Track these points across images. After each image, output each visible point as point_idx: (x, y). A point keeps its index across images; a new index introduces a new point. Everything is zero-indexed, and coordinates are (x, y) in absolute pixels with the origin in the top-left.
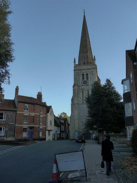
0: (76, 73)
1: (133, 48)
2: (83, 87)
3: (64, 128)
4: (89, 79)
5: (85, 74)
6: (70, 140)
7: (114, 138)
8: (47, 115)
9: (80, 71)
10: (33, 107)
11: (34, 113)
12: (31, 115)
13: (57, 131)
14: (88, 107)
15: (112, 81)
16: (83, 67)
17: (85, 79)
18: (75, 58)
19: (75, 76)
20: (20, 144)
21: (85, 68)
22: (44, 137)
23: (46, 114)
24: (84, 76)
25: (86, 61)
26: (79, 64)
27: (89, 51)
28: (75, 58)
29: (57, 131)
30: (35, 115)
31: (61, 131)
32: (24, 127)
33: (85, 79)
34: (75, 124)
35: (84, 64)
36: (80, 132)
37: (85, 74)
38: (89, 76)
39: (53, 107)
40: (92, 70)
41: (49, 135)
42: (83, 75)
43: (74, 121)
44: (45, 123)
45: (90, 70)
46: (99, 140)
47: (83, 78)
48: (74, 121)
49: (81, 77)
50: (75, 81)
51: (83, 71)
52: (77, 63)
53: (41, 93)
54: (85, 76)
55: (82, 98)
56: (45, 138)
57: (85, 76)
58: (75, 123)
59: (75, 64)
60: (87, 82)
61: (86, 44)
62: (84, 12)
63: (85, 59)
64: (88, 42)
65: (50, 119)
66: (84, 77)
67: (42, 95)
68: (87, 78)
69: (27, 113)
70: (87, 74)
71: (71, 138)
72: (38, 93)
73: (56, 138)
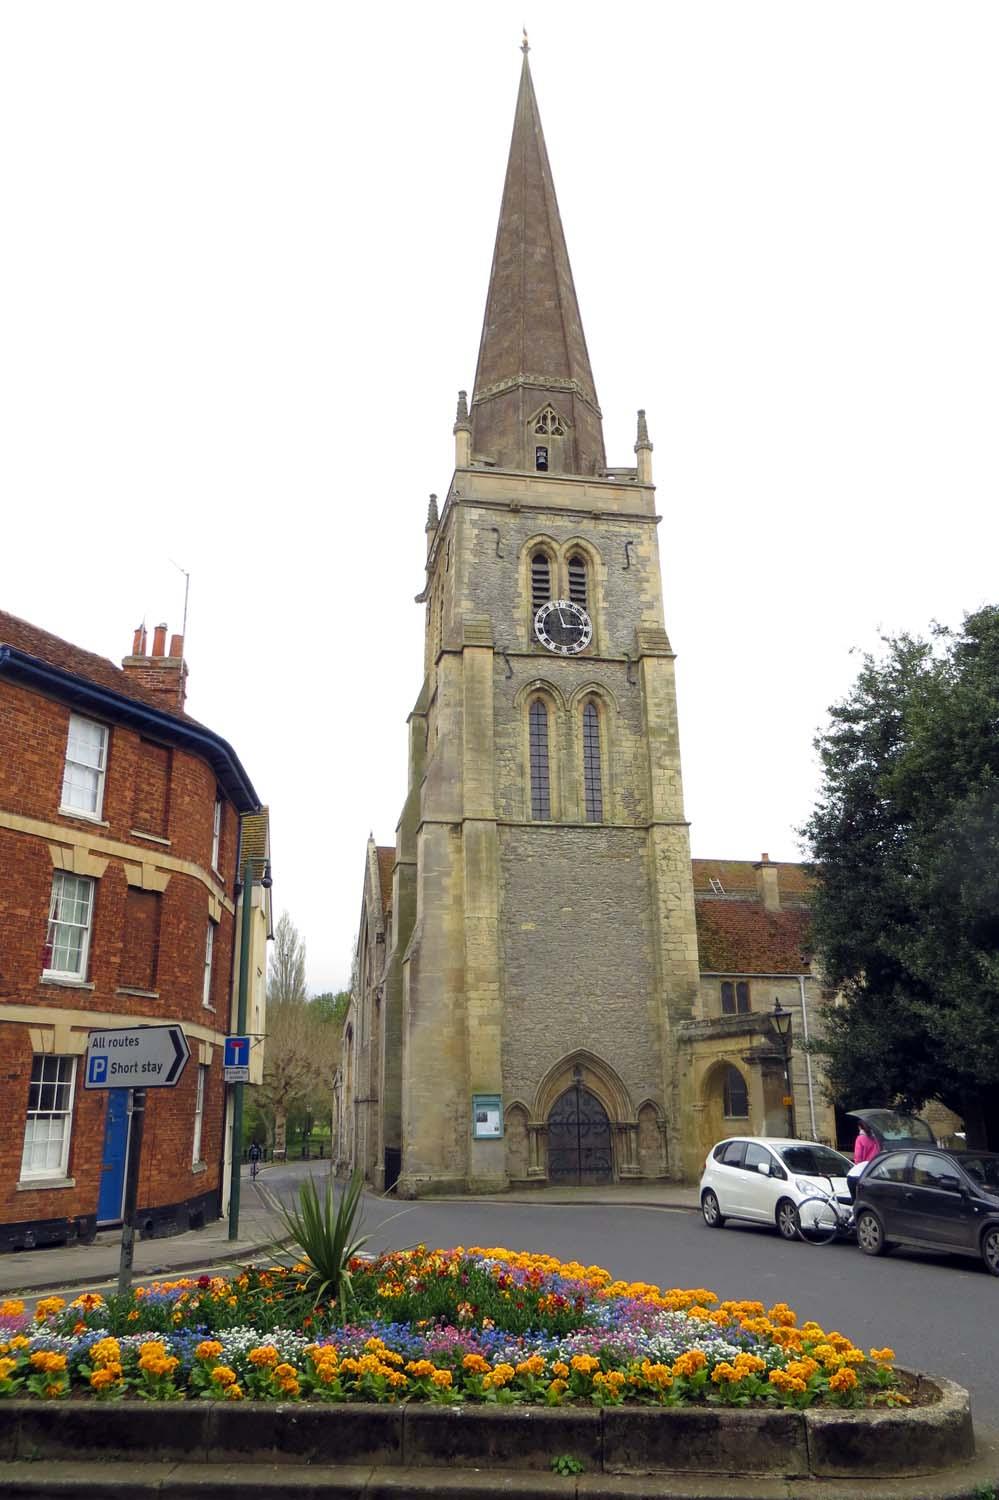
0: (474, 523)
2: (544, 668)
4: (597, 597)
5: (561, 550)
9: (512, 521)
10: (159, 785)
11: (167, 861)
12: (133, 876)
17: (560, 603)
18: (641, 413)
25: (555, 444)
28: (641, 413)
30: (172, 885)
32: (40, 1043)
38: (597, 573)
42: (540, 558)
45: (603, 527)
47: (541, 589)
49: (524, 572)
51: (544, 522)
53: (178, 641)
54: (559, 572)
57: (559, 572)
60: (574, 618)
62: (525, 48)
63: (550, 427)
64: (563, 289)
68: (578, 594)
69: (93, 841)
70: (577, 560)
72: (140, 633)
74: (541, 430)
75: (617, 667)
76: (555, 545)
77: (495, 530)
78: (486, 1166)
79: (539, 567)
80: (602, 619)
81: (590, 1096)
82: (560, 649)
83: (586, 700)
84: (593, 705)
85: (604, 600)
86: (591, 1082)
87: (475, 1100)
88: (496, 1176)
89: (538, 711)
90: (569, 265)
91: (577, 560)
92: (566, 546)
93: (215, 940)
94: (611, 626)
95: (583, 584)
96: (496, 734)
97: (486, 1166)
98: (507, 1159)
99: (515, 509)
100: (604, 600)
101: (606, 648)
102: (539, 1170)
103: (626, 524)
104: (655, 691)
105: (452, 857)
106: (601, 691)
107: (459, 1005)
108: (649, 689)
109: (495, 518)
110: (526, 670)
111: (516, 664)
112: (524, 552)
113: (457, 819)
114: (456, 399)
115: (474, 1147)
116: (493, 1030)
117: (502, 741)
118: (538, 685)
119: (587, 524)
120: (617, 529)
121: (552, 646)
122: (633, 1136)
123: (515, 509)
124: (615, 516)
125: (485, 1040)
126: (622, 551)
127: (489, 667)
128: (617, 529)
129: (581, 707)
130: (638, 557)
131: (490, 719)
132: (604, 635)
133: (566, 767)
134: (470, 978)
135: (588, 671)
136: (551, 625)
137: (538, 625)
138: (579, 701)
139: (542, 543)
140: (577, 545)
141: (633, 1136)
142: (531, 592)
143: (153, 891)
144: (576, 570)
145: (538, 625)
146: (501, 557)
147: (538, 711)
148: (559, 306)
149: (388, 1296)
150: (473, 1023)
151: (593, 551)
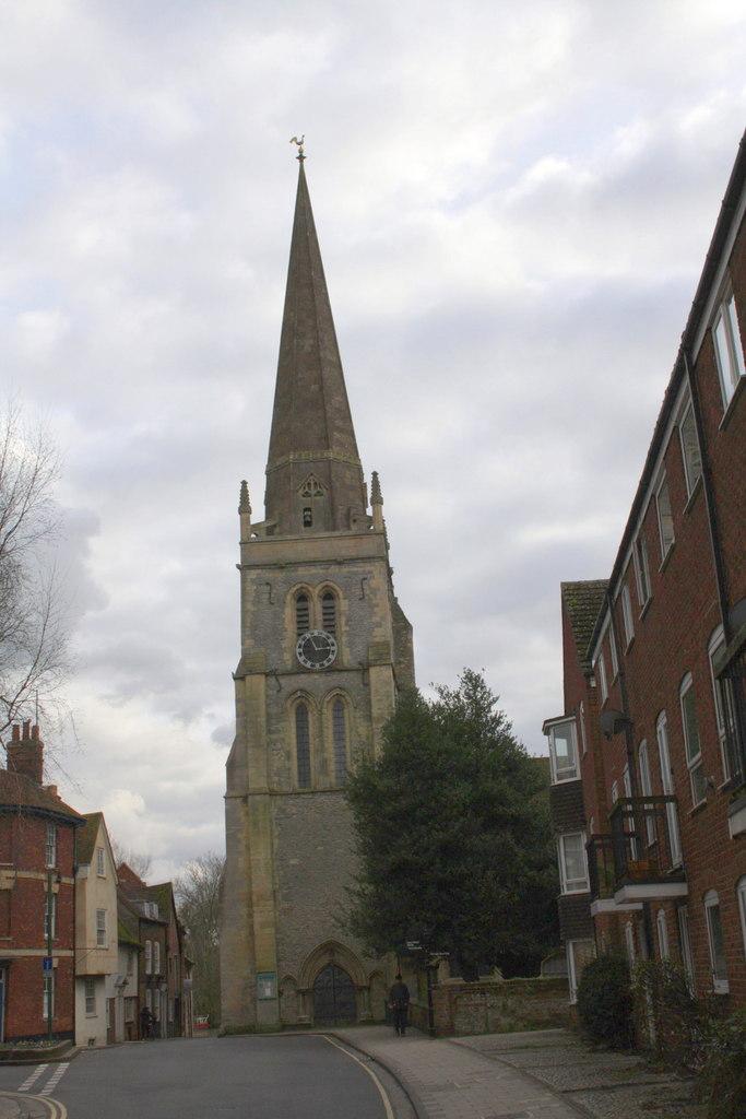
0: (253, 581)
1: (605, 573)
2: (303, 681)
3: (158, 953)
5: (315, 592)
6: (220, 1036)
7: (509, 1003)
8: (79, 875)
11: (11, 874)
13: (125, 983)
14: (360, 828)
15: (491, 681)
16: (301, 546)
17: (317, 631)
18: (244, 483)
19: (249, 606)
20: (31, 1054)
21: (312, 555)
22: (60, 1023)
23: (75, 871)
24: (311, 605)
26: (270, 529)
27: (341, 431)
28: (244, 483)
29: (125, 983)
30: (16, 887)
31: (148, 982)
33: (317, 631)
34: (252, 926)
35: (308, 524)
36: (289, 978)
37: (315, 592)
38: (343, 605)
39: (110, 821)
40: (358, 568)
41: (90, 1008)
42: (302, 598)
43: (250, 905)
44: (69, 931)
45: (345, 570)
46: (436, 1017)
47: (303, 623)
48: (250, 905)
49: (289, 613)
50: (248, 642)
51: (301, 571)
52: (258, 514)
53: (36, 729)
54: (316, 607)
55: (295, 754)
56: (69, 1028)
57: (316, 607)
58: (258, 919)
59: (245, 521)
61: (314, 387)
62: (301, 158)
65: (98, 897)
66: (311, 612)
67: (41, 746)
68: (330, 625)
70: (329, 596)
71: (229, 1017)
73: (120, 1031)
74: (306, 494)
75: (355, 674)
76: (310, 589)
77: (267, 584)
78: (266, 1016)
79: (300, 605)
80: (344, 639)
81: (342, 970)
82: (323, 665)
83: (334, 700)
84: (339, 707)
85: (346, 624)
86: (341, 960)
87: (259, 974)
88: (273, 1021)
89: (302, 713)
90: (336, 343)
91: (329, 596)
92: (320, 587)
93: (57, 902)
94: (351, 644)
95: (325, 620)
96: (269, 732)
97: (266, 1016)
98: (227, 1033)
99: (280, 566)
100: (346, 624)
101: (348, 658)
102: (305, 1017)
103: (361, 565)
104: (377, 691)
105: (243, 819)
106: (343, 693)
107: (250, 915)
108: (373, 689)
109: (268, 575)
110: (289, 683)
111: (283, 681)
112: (289, 597)
113: (243, 794)
114: (240, 487)
115: (259, 1004)
116: (270, 931)
117: (274, 737)
118: (299, 694)
119: (334, 569)
120: (356, 569)
121: (308, 665)
122: (366, 994)
123: (280, 566)
124: (353, 560)
125: (265, 936)
126: (359, 586)
127: (262, 686)
128: (356, 569)
129: (331, 706)
130: (370, 588)
131: (264, 725)
132: (346, 651)
133: (321, 749)
134: (254, 898)
135: (335, 679)
136: (307, 649)
137: (298, 650)
138: (328, 702)
139: (302, 588)
140: (327, 586)
141: (366, 994)
142: (296, 626)
143: (392, 586)
144: (328, 603)
145: (298, 650)
146: (267, 584)
147: (302, 713)
148: (321, 389)
149: (630, 982)
150: (256, 927)
151: (336, 587)
